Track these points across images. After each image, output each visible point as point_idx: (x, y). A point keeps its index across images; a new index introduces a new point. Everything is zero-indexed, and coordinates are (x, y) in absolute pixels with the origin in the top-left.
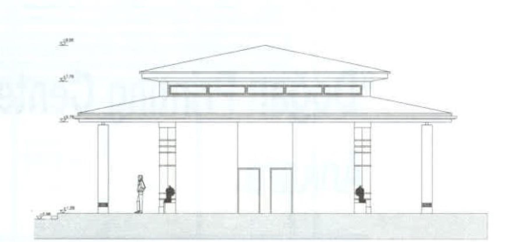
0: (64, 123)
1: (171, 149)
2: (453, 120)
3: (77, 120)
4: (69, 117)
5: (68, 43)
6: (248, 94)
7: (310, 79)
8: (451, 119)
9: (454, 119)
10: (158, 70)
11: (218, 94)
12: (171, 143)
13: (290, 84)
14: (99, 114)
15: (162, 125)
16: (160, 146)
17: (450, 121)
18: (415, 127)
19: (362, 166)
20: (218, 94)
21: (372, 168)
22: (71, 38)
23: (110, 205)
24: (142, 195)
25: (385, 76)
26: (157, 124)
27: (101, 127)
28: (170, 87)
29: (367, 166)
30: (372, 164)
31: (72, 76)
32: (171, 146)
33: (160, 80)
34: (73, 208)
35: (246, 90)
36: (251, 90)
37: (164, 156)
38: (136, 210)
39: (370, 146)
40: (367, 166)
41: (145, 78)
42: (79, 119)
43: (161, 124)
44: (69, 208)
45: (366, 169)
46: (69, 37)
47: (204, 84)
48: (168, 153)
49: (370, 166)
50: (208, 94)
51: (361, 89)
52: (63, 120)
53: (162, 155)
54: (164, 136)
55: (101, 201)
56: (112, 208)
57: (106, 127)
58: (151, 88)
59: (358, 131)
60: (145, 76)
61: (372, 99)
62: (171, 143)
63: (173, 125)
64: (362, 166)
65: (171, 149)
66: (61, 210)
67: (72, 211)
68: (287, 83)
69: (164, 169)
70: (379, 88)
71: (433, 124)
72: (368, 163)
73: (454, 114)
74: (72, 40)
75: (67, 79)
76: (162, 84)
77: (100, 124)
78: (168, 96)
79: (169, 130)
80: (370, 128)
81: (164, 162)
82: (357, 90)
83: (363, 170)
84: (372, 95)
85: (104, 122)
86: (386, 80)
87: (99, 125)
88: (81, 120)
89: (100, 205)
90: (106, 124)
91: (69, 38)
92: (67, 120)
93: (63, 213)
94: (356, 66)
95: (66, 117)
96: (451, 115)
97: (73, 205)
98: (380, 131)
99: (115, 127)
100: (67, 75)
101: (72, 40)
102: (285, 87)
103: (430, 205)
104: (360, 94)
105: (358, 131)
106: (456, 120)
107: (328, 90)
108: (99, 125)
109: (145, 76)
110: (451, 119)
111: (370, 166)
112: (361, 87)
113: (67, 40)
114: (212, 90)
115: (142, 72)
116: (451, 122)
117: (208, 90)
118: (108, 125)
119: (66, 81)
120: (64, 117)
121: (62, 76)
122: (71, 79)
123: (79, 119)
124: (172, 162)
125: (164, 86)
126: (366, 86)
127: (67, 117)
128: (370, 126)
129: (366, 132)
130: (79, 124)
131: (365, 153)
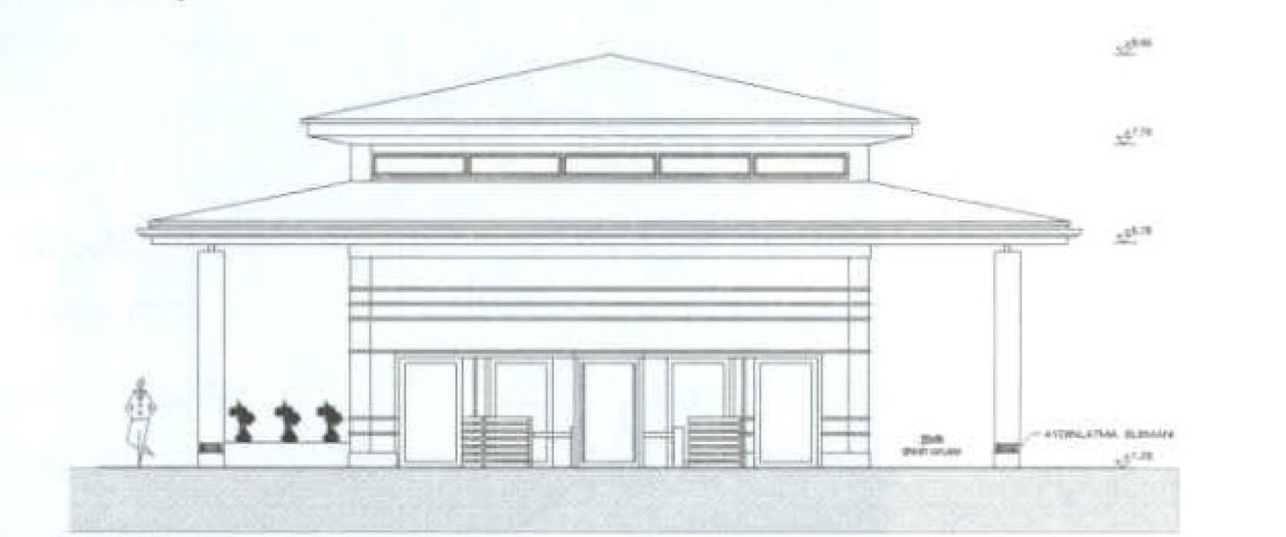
0: (1127, 246)
1: (857, 312)
2: (1072, 241)
3: (147, 241)
5: (1140, 50)
7: (723, 137)
8: (1067, 237)
9: (1076, 236)
10: (346, 115)
15: (355, 251)
17: (1062, 240)
18: (978, 256)
22: (1147, 36)
25: (903, 129)
27: (204, 256)
28: (375, 157)
29: (861, 352)
32: (363, 304)
35: (657, 165)
37: (360, 328)
39: (351, 304)
40: (861, 352)
41: (314, 137)
42: (152, 236)
44: (1139, 455)
45: (859, 361)
50: (468, 174)
53: (356, 325)
54: (361, 280)
55: (205, 439)
57: (219, 255)
58: (330, 161)
59: (361, 267)
60: (316, 129)
61: (357, 185)
63: (864, 251)
64: (848, 351)
65: (857, 312)
67: (1145, 463)
68: (565, 150)
70: (888, 161)
71: (1025, 250)
73: (1074, 226)
74: (1146, 43)
75: (1135, 139)
76: (357, 151)
78: (371, 181)
80: (869, 258)
81: (360, 341)
82: (836, 166)
83: (853, 363)
84: (874, 177)
85: (1009, 245)
86: (907, 140)
87: (996, 253)
88: (156, 240)
90: (1014, 248)
91: (1139, 37)
93: (1122, 468)
98: (893, 265)
99: (242, 257)
100: (1135, 130)
101: (1146, 43)
102: (657, 158)
103: (1013, 449)
104: (844, 175)
105: (361, 267)
106: (1079, 239)
107: (478, 165)
110: (1067, 237)
112: (844, 156)
113: (1134, 42)
114: (478, 165)
115: (308, 121)
123: (152, 236)
124: (859, 342)
126: (857, 156)
128: (867, 254)
129: (859, 266)
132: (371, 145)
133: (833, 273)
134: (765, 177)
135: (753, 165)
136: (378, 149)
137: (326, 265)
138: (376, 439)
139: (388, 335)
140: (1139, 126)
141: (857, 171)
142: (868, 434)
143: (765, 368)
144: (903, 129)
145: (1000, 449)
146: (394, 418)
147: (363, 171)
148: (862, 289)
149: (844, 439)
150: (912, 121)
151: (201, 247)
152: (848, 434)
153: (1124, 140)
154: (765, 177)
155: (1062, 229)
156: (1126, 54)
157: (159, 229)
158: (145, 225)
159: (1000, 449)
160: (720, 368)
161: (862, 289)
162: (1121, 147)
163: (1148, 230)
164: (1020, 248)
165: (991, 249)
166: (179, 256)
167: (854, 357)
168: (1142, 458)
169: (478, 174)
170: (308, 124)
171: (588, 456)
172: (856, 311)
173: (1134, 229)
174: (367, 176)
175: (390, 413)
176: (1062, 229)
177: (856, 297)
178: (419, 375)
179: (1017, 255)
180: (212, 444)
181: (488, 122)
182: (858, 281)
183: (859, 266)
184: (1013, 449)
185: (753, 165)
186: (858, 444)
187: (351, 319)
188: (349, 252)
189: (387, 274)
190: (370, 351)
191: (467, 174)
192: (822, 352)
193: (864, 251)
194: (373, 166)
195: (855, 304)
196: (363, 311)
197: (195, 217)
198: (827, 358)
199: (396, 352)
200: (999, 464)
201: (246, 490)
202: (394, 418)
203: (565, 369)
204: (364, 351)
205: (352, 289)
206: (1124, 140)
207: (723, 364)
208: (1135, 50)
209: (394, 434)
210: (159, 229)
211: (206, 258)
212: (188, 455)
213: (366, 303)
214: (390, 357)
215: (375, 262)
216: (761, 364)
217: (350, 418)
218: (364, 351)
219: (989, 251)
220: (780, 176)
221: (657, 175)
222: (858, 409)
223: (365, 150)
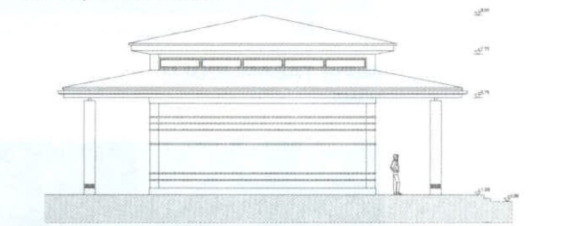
2: (463, 96)
3: (62, 96)
4: (484, 92)
6: (244, 68)
9: (466, 94)
13: (249, 56)
15: (152, 101)
16: (375, 124)
17: (460, 96)
18: (422, 103)
21: (377, 146)
22: (487, 8)
23: (442, 186)
25: (390, 48)
26: (148, 99)
27: (433, 103)
28: (161, 60)
30: (377, 142)
31: (487, 48)
32: (369, 124)
34: (488, 190)
35: (201, 63)
37: (154, 134)
43: (151, 99)
44: (484, 189)
45: (371, 148)
47: (236, 56)
48: (366, 130)
49: (375, 144)
51: (365, 63)
54: (154, 113)
56: (445, 189)
57: (93, 103)
58: (141, 61)
59: (154, 108)
60: (135, 48)
69: (154, 148)
70: (384, 61)
73: (465, 89)
77: (433, 99)
78: (159, 70)
81: (154, 140)
82: (361, 63)
86: (391, 53)
87: (431, 101)
88: (66, 96)
90: (93, 99)
92: (482, 96)
96: (462, 90)
97: (487, 187)
101: (487, 10)
103: (93, 186)
106: (466, 96)
108: (431, 101)
109: (135, 48)
111: (375, 144)
112: (365, 59)
114: (330, 64)
115: (132, 44)
116: (461, 98)
118: (441, 101)
124: (371, 140)
125: (155, 59)
128: (374, 102)
131: (369, 130)
132: (159, 54)
133: (359, 110)
134: (247, 68)
136: (162, 56)
137: (140, 106)
139: (165, 137)
141: (370, 66)
142: (375, 180)
144: (390, 48)
145: (432, 186)
146: (374, 173)
148: (372, 117)
150: (394, 44)
154: (247, 68)
155: (458, 91)
156: (479, 15)
157: (65, 91)
158: (61, 89)
159: (432, 186)
161: (372, 117)
169: (247, 67)
170: (131, 46)
173: (482, 92)
174: (157, 68)
176: (458, 91)
177: (370, 120)
182: (370, 114)
186: (370, 184)
189: (165, 110)
190: (367, 144)
191: (325, 67)
195: (369, 123)
197: (89, 85)
200: (86, 193)
201: (369, 203)
204: (362, 144)
205: (150, 117)
206: (478, 52)
208: (482, 13)
210: (65, 91)
211: (87, 103)
213: (156, 123)
215: (161, 105)
218: (362, 144)
222: (371, 169)
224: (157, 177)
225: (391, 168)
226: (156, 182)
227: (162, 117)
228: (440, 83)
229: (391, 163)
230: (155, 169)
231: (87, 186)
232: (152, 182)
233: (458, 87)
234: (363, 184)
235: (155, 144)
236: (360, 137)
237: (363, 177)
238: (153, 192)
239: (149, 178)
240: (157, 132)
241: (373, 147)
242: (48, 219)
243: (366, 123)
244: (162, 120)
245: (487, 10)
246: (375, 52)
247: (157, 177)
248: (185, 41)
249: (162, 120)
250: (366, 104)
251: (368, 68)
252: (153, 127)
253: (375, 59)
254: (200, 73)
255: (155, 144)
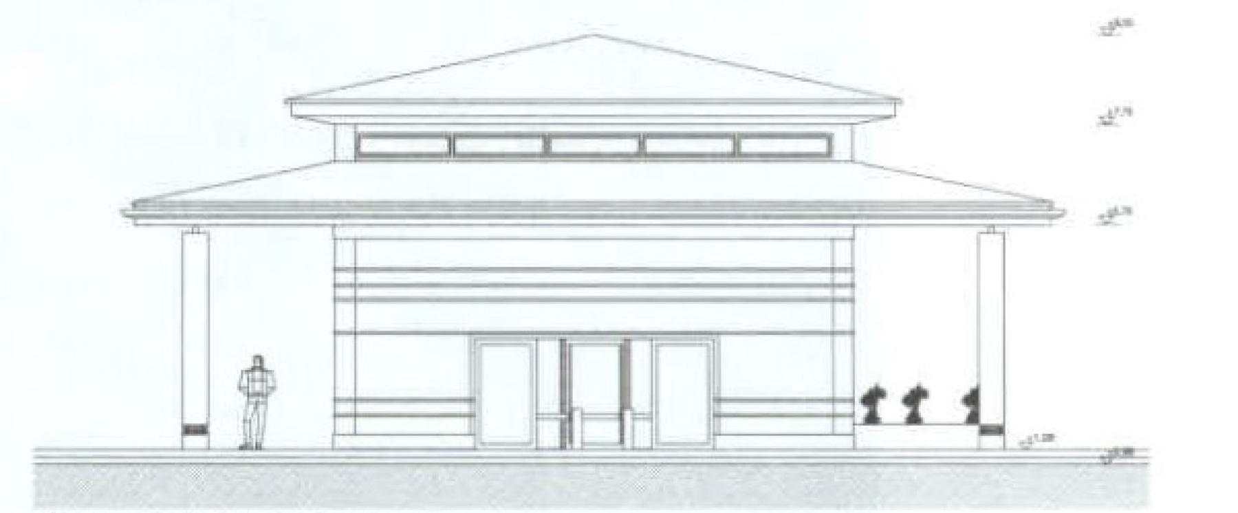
0: (1108, 227)
2: (1054, 222)
3: (130, 221)
6: (646, 155)
10: (340, 94)
11: (765, 157)
12: (842, 278)
14: (185, 205)
15: (340, 232)
17: (1046, 222)
19: (833, 333)
20: (765, 157)
23: (211, 429)
24: (266, 403)
25: (888, 110)
27: (188, 238)
28: (358, 138)
31: (1129, 111)
32: (841, 286)
33: (338, 120)
34: (1050, 437)
36: (747, 146)
37: (346, 309)
38: (241, 442)
41: (301, 117)
44: (1040, 437)
45: (843, 342)
46: (1122, 16)
52: (1107, 219)
54: (346, 260)
57: (203, 238)
58: (313, 141)
60: (299, 109)
62: (842, 278)
63: (847, 232)
64: (833, 333)
66: (1022, 443)
67: (1048, 445)
69: (346, 342)
70: (876, 141)
71: (211, 229)
72: (847, 328)
73: (1057, 206)
79: (837, 243)
80: (852, 239)
81: (345, 324)
82: (819, 146)
85: (993, 226)
86: (886, 122)
88: (140, 221)
89: (188, 430)
92: (1117, 219)
94: (819, 87)
95: (1113, 213)
98: (878, 247)
99: (226, 237)
100: (1117, 110)
101: (1128, 23)
102: (547, 139)
103: (202, 430)
104: (828, 155)
112: (829, 138)
115: (291, 101)
117: (642, 144)
119: (1117, 125)
120: (1109, 212)
121: (1105, 112)
122: (1126, 117)
124: (843, 323)
127: (1116, 210)
129: (843, 248)
130: (133, 227)
133: (818, 255)
135: (737, 145)
136: (361, 129)
137: (312, 243)
138: (839, 421)
139: (370, 315)
140: (1121, 106)
141: (841, 150)
143: (662, 349)
144: (888, 110)
146: (470, 400)
147: (347, 151)
149: (828, 421)
150: (895, 101)
151: (185, 229)
152: (833, 416)
153: (1107, 121)
155: (1043, 210)
157: (142, 211)
160: (704, 349)
162: (1103, 127)
163: (1128, 211)
164: (207, 229)
165: (975, 230)
166: (164, 237)
167: (838, 338)
168: (1044, 440)
171: (526, 439)
172: (840, 293)
173: (1116, 210)
175: (465, 394)
176: (1043, 210)
178: (492, 355)
179: (1000, 237)
180: (195, 426)
181: (486, 102)
183: (843, 248)
184: (202, 430)
185: (737, 145)
187: (336, 300)
188: (333, 234)
189: (370, 255)
191: (452, 153)
192: (719, 333)
193: (847, 232)
194: (357, 147)
195: (837, 285)
196: (348, 293)
198: (723, 338)
199: (470, 333)
202: (470, 400)
203: (550, 350)
204: (363, 333)
206: (1107, 121)
207: (707, 345)
208: (1118, 30)
209: (471, 416)
210: (142, 211)
212: (173, 436)
213: (351, 285)
214: (463, 340)
216: (657, 346)
217: (852, 401)
219: (177, 232)
220: (768, 154)
221: (736, 155)
223: (350, 130)
224: (350, 406)
225: (240, 388)
226: (350, 421)
227: (364, 270)
228: (1009, 193)
229: (238, 379)
230: (346, 391)
231: (188, 430)
232: (340, 421)
233: (1044, 201)
234: (824, 425)
235: (843, 333)
236: (817, 316)
237: (826, 408)
238: (342, 442)
239: (331, 411)
240: (351, 306)
241: (847, 338)
242: (38, 505)
243: (833, 286)
244: (363, 278)
245: (1128, 23)
246: (852, 120)
247: (350, 406)
248: (428, 94)
249: (363, 278)
250: (833, 239)
251: (836, 156)
252: (342, 292)
253: (852, 133)
254: (641, 167)
255: (843, 333)
